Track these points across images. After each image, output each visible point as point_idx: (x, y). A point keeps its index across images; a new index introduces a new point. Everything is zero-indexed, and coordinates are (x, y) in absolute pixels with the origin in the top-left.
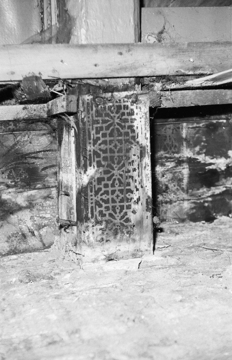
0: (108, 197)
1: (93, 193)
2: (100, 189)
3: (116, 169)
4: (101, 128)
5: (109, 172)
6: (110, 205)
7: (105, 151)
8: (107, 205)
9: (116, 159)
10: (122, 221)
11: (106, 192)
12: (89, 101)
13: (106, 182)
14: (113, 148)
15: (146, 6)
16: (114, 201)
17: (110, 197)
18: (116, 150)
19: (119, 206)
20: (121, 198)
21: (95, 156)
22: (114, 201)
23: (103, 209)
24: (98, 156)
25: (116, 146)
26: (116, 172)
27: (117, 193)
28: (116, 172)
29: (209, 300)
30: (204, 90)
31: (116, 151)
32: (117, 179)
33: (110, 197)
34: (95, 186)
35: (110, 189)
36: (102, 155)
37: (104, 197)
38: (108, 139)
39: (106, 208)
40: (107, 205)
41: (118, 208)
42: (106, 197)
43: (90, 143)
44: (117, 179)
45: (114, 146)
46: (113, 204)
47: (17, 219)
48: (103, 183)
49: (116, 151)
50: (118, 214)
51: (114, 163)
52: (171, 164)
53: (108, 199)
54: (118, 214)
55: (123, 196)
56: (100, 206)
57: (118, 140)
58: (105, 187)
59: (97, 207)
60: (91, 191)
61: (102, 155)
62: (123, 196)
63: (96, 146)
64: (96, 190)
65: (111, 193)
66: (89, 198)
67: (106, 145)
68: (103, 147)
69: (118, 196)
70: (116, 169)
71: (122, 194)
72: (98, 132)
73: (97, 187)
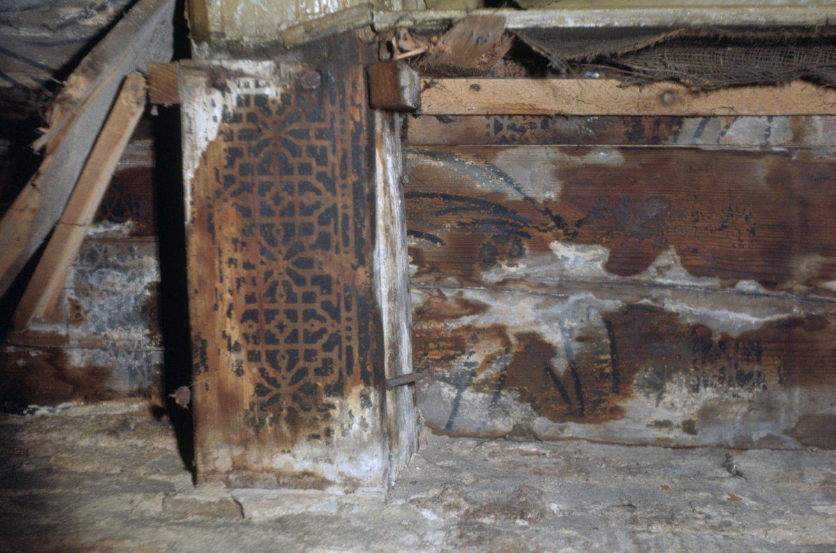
0: (307, 326)
4: (312, 150)
8: (310, 306)
10: (275, 391)
13: (311, 366)
15: (175, 101)
16: (292, 315)
17: (301, 326)
18: (277, 210)
20: (277, 337)
22: (292, 315)
23: (317, 169)
24: (326, 306)
25: (277, 200)
27: (282, 337)
31: (277, 212)
32: (281, 284)
33: (301, 326)
34: (336, 232)
36: (317, 307)
37: (317, 326)
38: (298, 219)
39: (314, 353)
40: (310, 306)
41: (281, 296)
42: (312, 325)
43: (344, 187)
44: (281, 284)
48: (319, 364)
49: (277, 212)
51: (285, 284)
52: (126, 321)
55: (267, 327)
56: (326, 306)
57: (275, 341)
58: (314, 353)
59: (335, 304)
60: (345, 217)
62: (267, 327)
63: (330, 205)
66: (355, 326)
67: (302, 205)
68: (309, 198)
69: (281, 327)
71: (269, 331)
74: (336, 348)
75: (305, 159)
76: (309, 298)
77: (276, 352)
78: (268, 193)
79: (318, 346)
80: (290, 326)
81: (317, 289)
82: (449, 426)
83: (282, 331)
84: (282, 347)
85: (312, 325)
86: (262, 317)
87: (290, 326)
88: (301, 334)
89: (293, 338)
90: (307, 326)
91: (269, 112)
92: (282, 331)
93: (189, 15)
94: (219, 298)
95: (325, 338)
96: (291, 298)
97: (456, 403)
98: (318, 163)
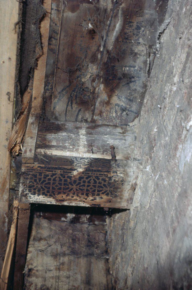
1: (98, 175)
2: (99, 179)
3: (72, 187)
5: (40, 181)
6: (86, 184)
7: (89, 182)
9: (83, 188)
11: (61, 180)
12: (72, 173)
14: (56, 185)
16: (88, 186)
19: (98, 188)
21: (87, 176)
22: (88, 186)
24: (87, 178)
26: (74, 186)
28: (74, 186)
29: (44, 230)
30: (120, 213)
31: (60, 186)
41: (99, 189)
45: (57, 185)
46: (97, 186)
47: (50, 79)
49: (60, 186)
50: (103, 189)
53: (90, 183)
54: (103, 189)
55: (91, 191)
56: (87, 178)
61: (87, 180)
62: (91, 191)
63: (60, 175)
64: (99, 177)
65: (88, 185)
69: (91, 188)
70: (72, 187)
72: (103, 179)
73: (101, 178)
76: (84, 182)
84: (85, 188)
85: (92, 182)
88: (90, 184)
96: (84, 186)
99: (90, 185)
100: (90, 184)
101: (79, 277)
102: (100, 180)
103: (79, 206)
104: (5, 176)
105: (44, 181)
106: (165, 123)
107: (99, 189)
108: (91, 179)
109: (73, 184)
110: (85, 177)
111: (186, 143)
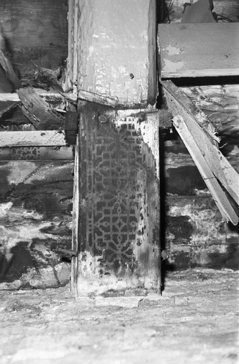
0: (108, 224)
2: (100, 216)
16: (115, 229)
17: (111, 224)
23: (102, 237)
24: (100, 234)
27: (120, 229)
33: (111, 224)
35: (111, 216)
36: (104, 233)
41: (119, 211)
42: (106, 224)
48: (103, 208)
53: (109, 226)
56: (100, 234)
58: (105, 236)
69: (120, 224)
74: (96, 215)
75: (107, 242)
76: (108, 237)
77: (122, 213)
78: (122, 220)
79: (104, 216)
80: (116, 224)
81: (104, 241)
82: (59, 283)
83: (120, 226)
84: (119, 233)
85: (106, 224)
86: (128, 220)
87: (116, 224)
88: (111, 221)
89: (115, 219)
90: (108, 224)
91: (117, 132)
92: (120, 226)
93: (156, 93)
94: (146, 211)
95: (100, 219)
96: (115, 236)
97: (55, 273)
98: (101, 240)
99: (114, 226)
100: (111, 227)
101: (170, 260)
102: (102, 156)
103: (182, 78)
104: (120, 337)
105: (100, 160)
106: (71, 322)
107: (119, 238)
108: (101, 226)
109: (114, 198)
110: (97, 237)
111: (8, 229)
